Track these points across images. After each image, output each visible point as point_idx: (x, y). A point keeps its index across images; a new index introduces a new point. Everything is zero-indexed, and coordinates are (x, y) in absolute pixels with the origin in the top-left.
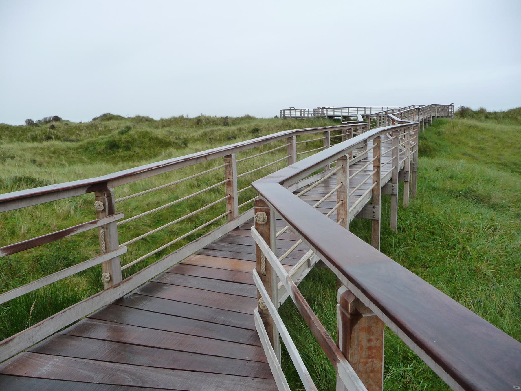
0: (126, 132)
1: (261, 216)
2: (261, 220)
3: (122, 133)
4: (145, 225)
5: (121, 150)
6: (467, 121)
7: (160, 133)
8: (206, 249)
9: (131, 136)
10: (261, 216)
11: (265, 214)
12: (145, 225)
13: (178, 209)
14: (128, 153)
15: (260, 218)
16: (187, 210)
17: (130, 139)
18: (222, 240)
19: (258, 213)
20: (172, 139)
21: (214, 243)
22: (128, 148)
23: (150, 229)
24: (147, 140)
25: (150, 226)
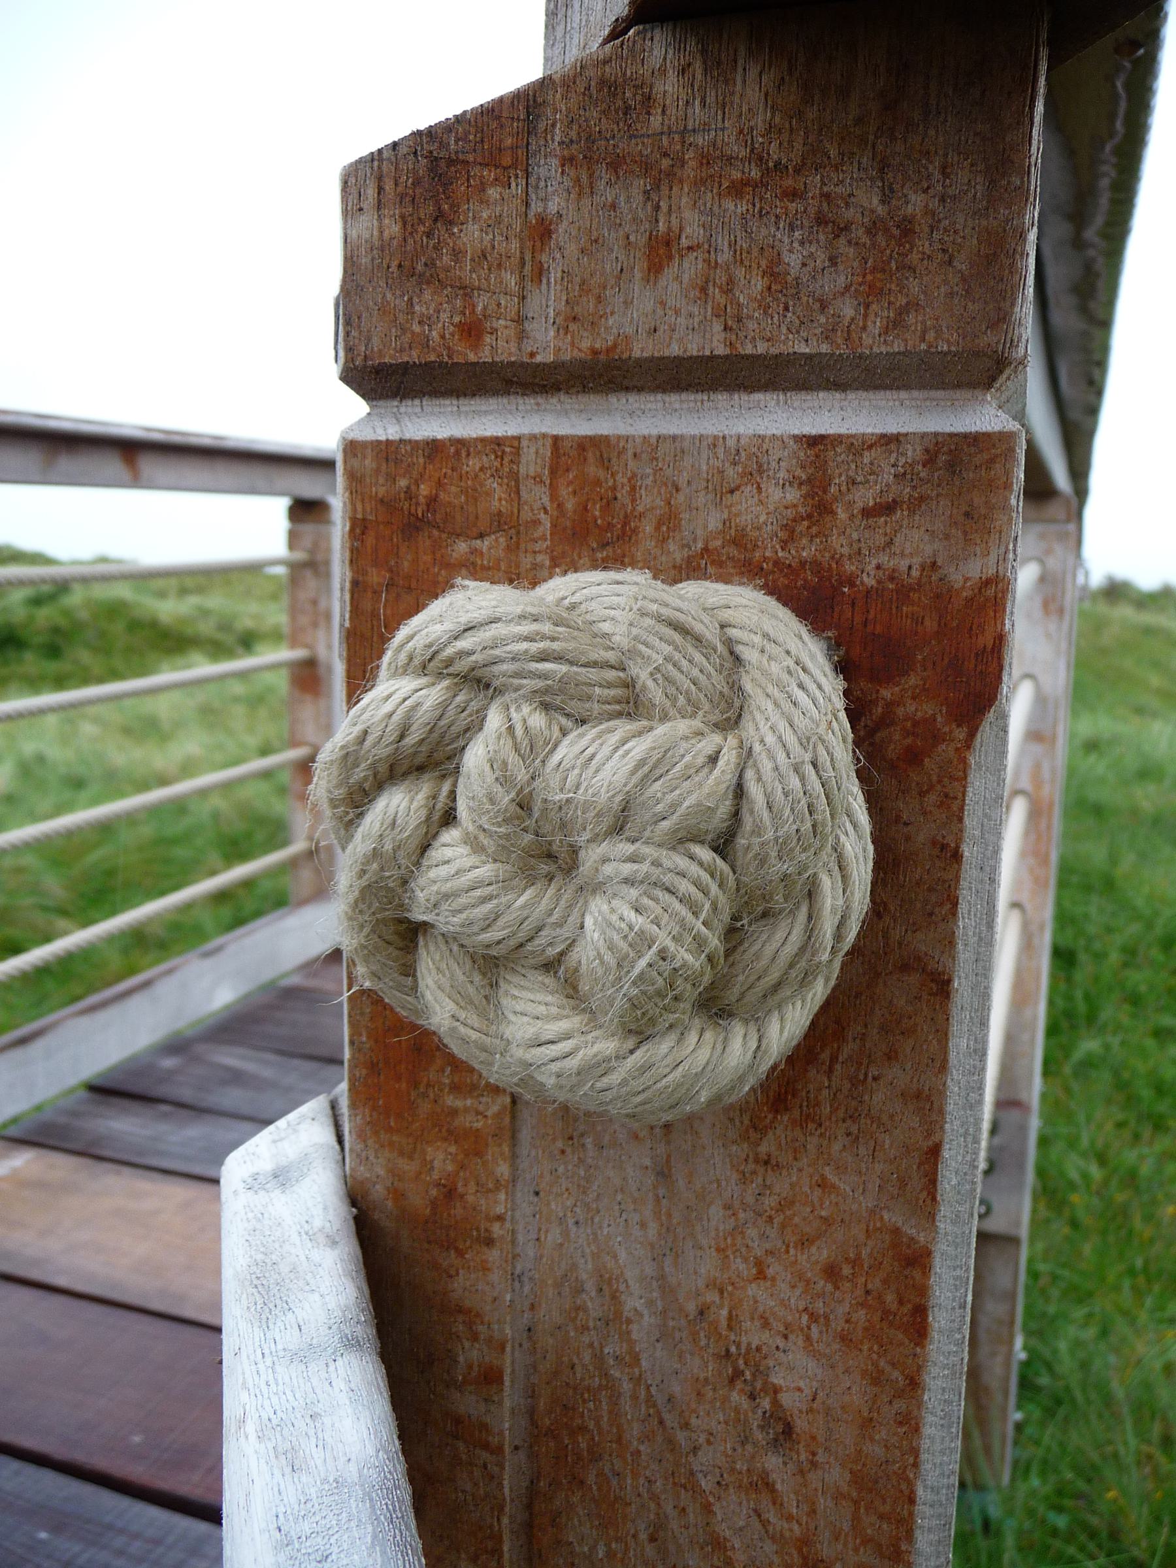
0: (52, 598)
1: (598, 762)
2: (621, 918)
3: (37, 601)
4: (45, 909)
5: (29, 656)
6: (1125, 612)
7: (168, 609)
8: (106, 1091)
9: (67, 613)
10: (598, 762)
11: (797, 690)
12: (45, 909)
13: (180, 852)
14: (52, 667)
15: (543, 846)
16: (214, 858)
17: (62, 622)
18: (235, 1027)
19: (467, 611)
20: (206, 628)
21: (177, 1046)
22: (53, 651)
23: (62, 923)
24: (119, 627)
25: (63, 912)
